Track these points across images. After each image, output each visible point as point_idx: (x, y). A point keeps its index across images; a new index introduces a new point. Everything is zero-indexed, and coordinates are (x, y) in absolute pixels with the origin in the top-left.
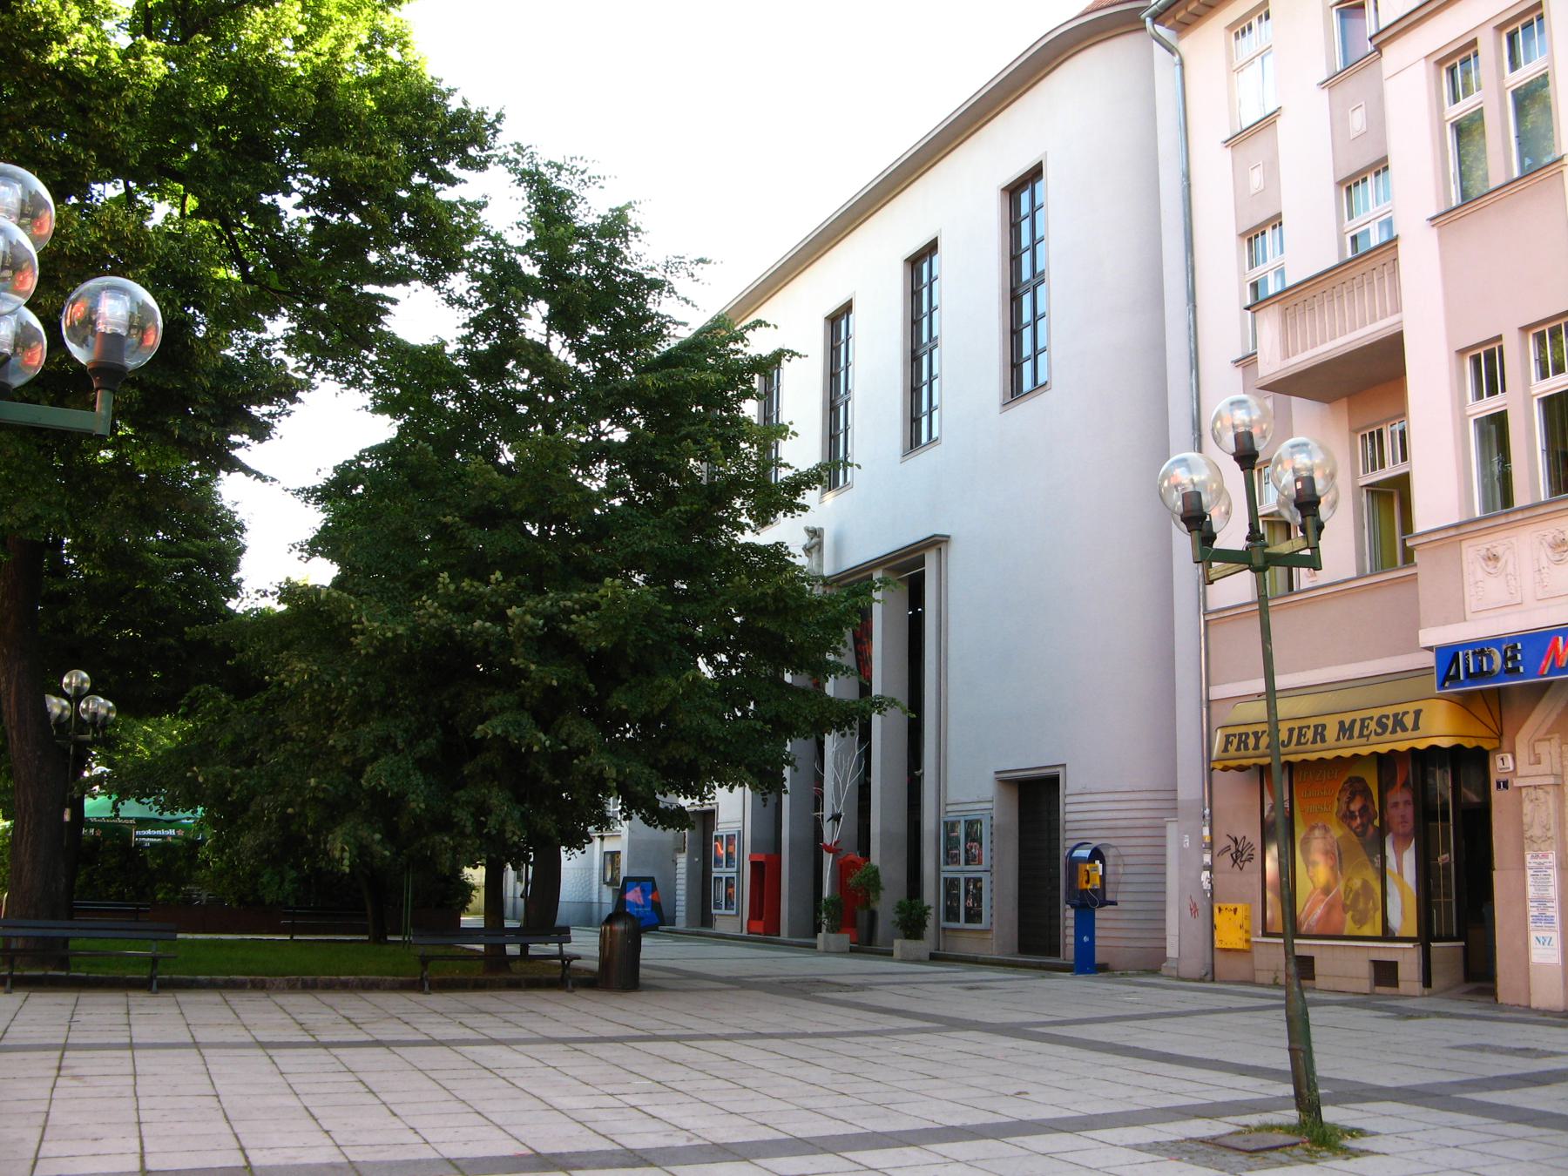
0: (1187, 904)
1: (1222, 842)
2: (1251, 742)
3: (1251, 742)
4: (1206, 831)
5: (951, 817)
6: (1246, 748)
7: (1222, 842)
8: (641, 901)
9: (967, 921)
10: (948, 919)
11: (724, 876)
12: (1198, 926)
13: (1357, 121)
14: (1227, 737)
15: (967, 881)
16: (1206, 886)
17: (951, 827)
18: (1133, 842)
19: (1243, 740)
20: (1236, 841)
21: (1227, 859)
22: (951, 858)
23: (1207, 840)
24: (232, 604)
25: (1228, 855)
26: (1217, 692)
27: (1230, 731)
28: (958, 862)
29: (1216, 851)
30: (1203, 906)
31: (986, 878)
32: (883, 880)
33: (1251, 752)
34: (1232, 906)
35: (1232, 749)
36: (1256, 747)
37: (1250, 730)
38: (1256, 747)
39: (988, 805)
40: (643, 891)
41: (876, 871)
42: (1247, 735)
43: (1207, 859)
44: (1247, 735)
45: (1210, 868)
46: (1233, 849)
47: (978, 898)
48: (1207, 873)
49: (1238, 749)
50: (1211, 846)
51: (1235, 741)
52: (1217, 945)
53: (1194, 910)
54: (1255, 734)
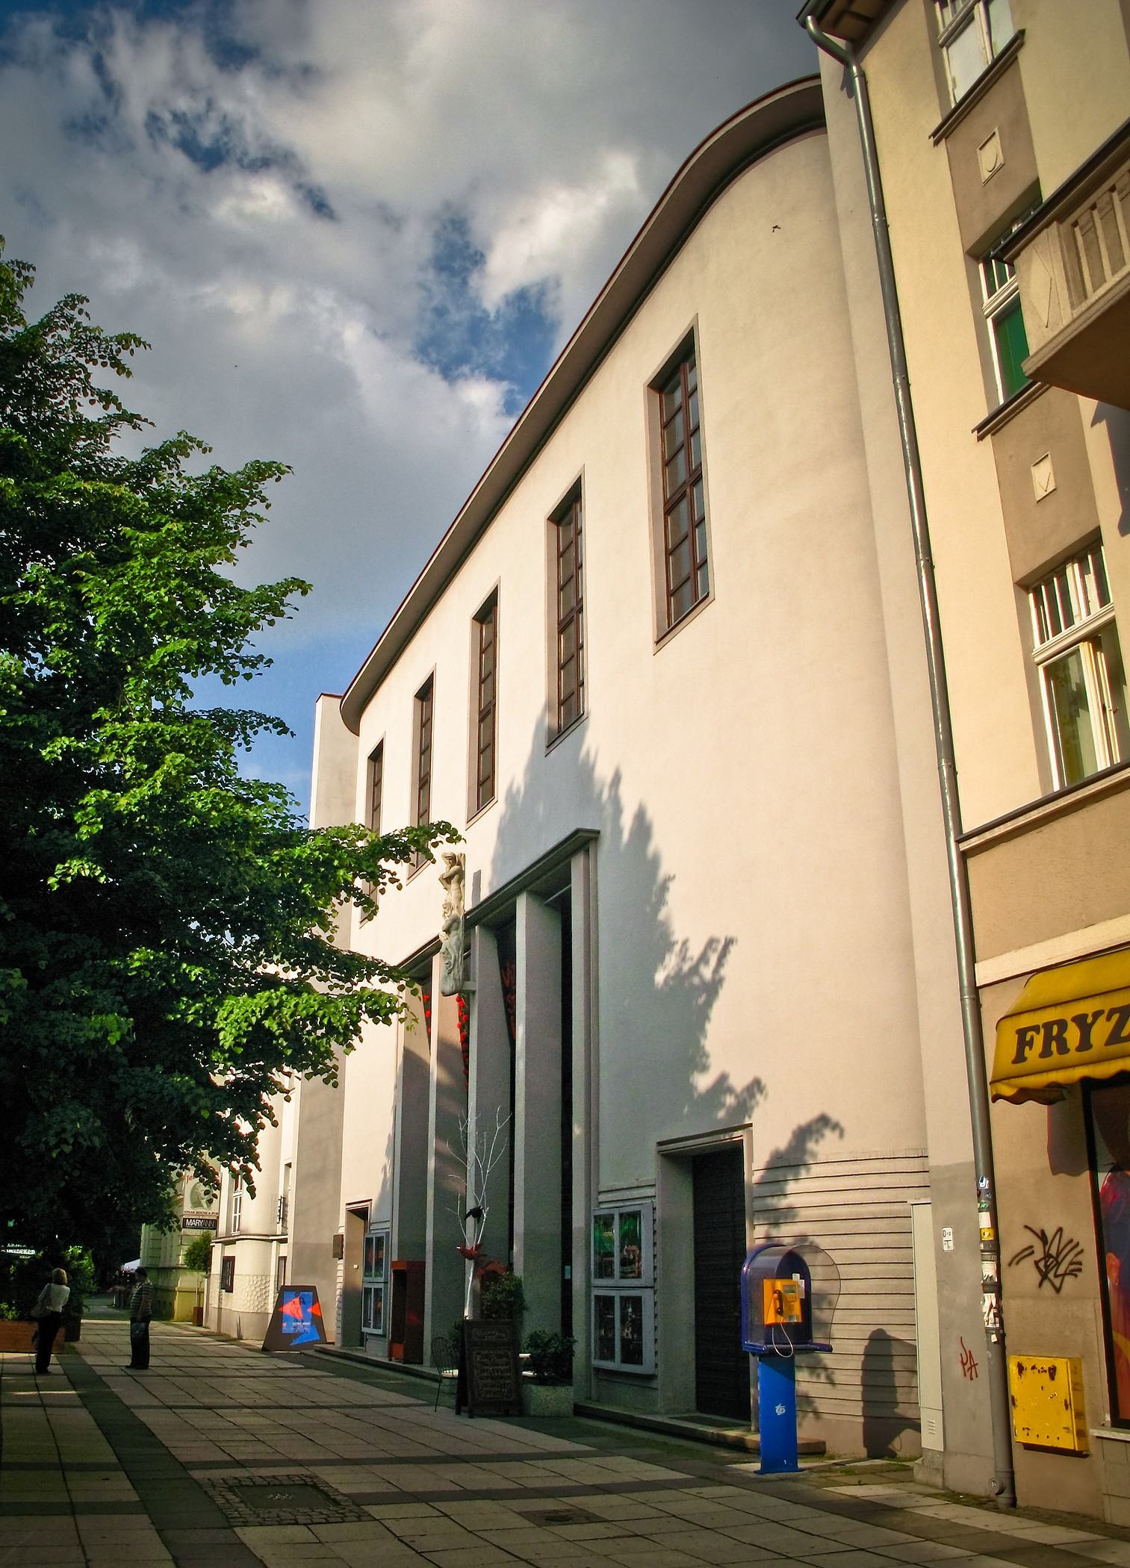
0: (955, 1351)
1: (1015, 1241)
2: (1073, 1035)
3: (1073, 1035)
4: (985, 1220)
5: (603, 1211)
6: (1063, 1049)
7: (1015, 1241)
8: (300, 1314)
9: (624, 1361)
10: (603, 1357)
11: (616, 1280)
12: (981, 1392)
13: (1043, 477)
14: (1022, 1033)
15: (625, 1300)
16: (990, 1320)
17: (605, 1222)
18: (858, 1241)
19: (1054, 1034)
20: (1042, 1237)
21: (1025, 1275)
22: (604, 1269)
23: (988, 1236)
24: (264, 1095)
25: (1028, 1264)
26: (985, 973)
27: (1026, 1021)
28: (611, 1275)
29: (1006, 1256)
30: (985, 1358)
31: (647, 1297)
32: (528, 1296)
33: (1073, 1055)
34: (1045, 1363)
35: (1032, 1054)
36: (1085, 1044)
37: (1068, 1013)
38: (1085, 1044)
39: (650, 1192)
40: (302, 1302)
41: (519, 1285)
42: (1062, 1025)
43: (989, 1269)
44: (1062, 1025)
45: (996, 1287)
46: (1039, 1254)
47: (637, 1326)
48: (990, 1299)
49: (1046, 1053)
50: (995, 1248)
51: (1039, 1040)
52: (1020, 1437)
53: (969, 1364)
54: (1080, 1020)
